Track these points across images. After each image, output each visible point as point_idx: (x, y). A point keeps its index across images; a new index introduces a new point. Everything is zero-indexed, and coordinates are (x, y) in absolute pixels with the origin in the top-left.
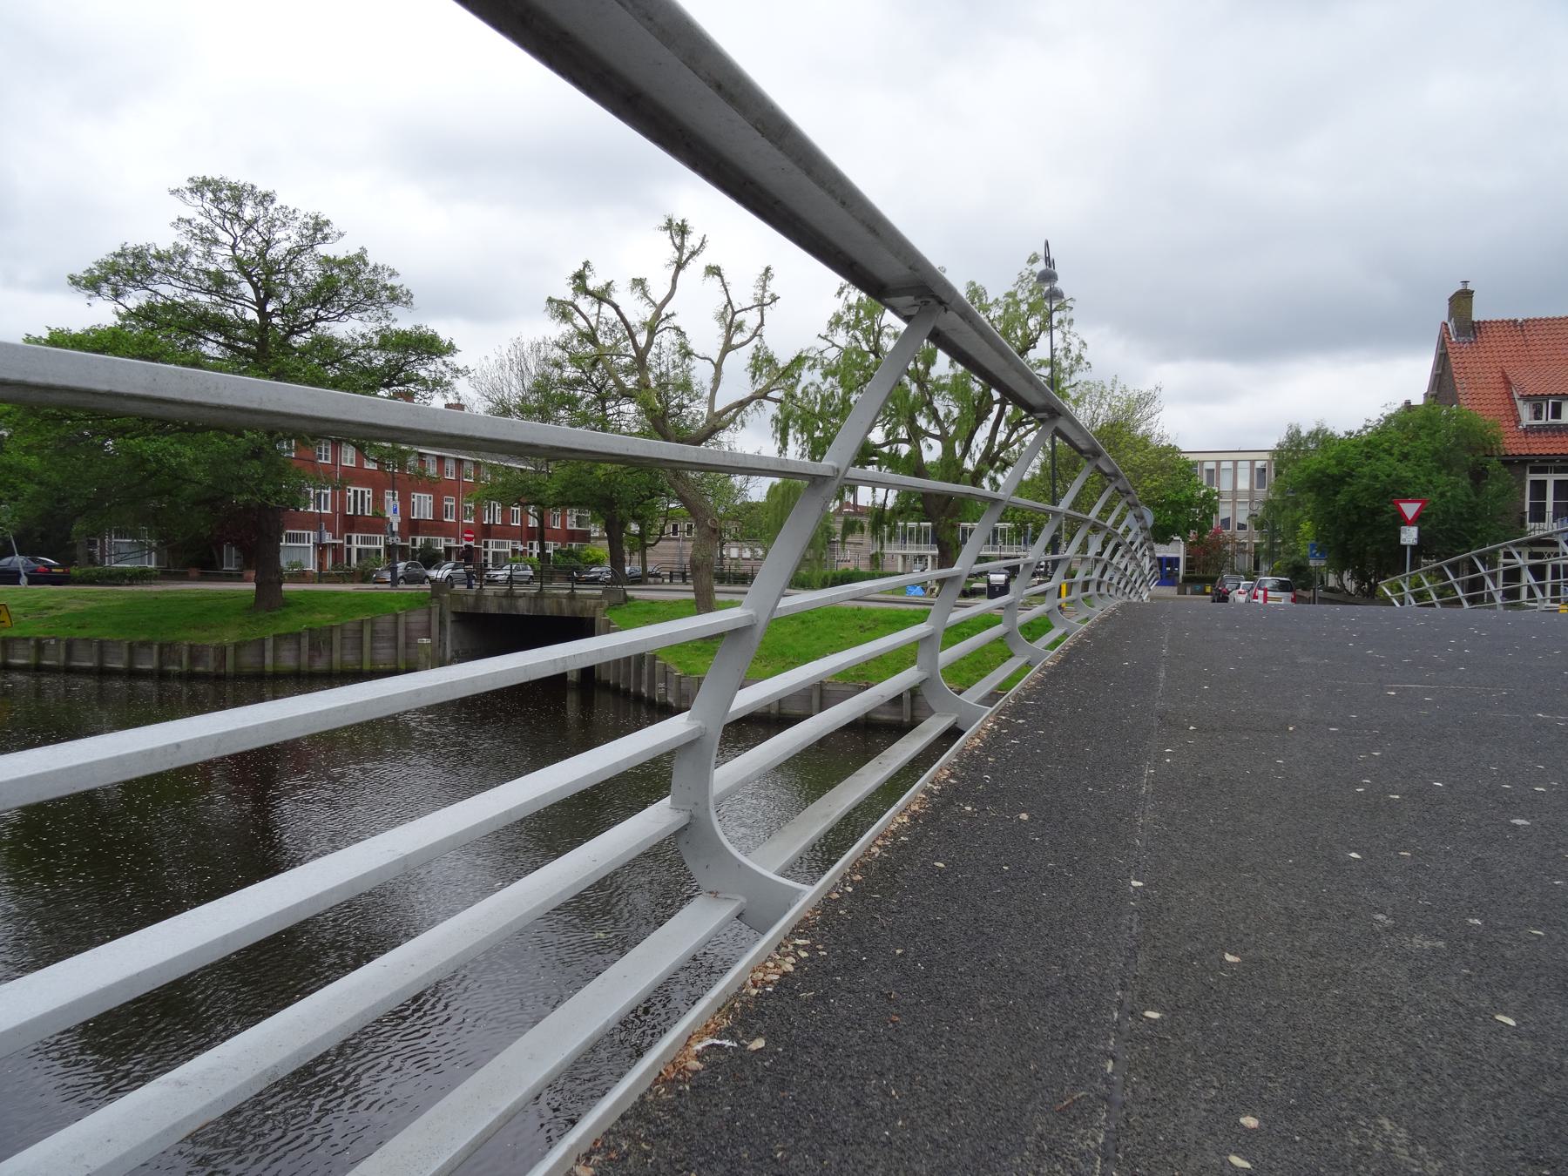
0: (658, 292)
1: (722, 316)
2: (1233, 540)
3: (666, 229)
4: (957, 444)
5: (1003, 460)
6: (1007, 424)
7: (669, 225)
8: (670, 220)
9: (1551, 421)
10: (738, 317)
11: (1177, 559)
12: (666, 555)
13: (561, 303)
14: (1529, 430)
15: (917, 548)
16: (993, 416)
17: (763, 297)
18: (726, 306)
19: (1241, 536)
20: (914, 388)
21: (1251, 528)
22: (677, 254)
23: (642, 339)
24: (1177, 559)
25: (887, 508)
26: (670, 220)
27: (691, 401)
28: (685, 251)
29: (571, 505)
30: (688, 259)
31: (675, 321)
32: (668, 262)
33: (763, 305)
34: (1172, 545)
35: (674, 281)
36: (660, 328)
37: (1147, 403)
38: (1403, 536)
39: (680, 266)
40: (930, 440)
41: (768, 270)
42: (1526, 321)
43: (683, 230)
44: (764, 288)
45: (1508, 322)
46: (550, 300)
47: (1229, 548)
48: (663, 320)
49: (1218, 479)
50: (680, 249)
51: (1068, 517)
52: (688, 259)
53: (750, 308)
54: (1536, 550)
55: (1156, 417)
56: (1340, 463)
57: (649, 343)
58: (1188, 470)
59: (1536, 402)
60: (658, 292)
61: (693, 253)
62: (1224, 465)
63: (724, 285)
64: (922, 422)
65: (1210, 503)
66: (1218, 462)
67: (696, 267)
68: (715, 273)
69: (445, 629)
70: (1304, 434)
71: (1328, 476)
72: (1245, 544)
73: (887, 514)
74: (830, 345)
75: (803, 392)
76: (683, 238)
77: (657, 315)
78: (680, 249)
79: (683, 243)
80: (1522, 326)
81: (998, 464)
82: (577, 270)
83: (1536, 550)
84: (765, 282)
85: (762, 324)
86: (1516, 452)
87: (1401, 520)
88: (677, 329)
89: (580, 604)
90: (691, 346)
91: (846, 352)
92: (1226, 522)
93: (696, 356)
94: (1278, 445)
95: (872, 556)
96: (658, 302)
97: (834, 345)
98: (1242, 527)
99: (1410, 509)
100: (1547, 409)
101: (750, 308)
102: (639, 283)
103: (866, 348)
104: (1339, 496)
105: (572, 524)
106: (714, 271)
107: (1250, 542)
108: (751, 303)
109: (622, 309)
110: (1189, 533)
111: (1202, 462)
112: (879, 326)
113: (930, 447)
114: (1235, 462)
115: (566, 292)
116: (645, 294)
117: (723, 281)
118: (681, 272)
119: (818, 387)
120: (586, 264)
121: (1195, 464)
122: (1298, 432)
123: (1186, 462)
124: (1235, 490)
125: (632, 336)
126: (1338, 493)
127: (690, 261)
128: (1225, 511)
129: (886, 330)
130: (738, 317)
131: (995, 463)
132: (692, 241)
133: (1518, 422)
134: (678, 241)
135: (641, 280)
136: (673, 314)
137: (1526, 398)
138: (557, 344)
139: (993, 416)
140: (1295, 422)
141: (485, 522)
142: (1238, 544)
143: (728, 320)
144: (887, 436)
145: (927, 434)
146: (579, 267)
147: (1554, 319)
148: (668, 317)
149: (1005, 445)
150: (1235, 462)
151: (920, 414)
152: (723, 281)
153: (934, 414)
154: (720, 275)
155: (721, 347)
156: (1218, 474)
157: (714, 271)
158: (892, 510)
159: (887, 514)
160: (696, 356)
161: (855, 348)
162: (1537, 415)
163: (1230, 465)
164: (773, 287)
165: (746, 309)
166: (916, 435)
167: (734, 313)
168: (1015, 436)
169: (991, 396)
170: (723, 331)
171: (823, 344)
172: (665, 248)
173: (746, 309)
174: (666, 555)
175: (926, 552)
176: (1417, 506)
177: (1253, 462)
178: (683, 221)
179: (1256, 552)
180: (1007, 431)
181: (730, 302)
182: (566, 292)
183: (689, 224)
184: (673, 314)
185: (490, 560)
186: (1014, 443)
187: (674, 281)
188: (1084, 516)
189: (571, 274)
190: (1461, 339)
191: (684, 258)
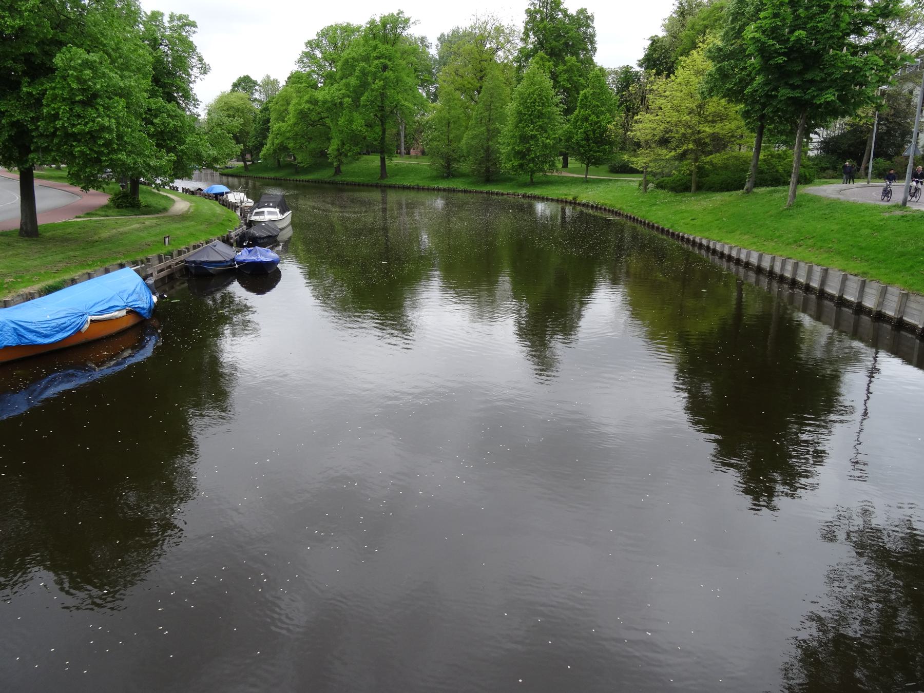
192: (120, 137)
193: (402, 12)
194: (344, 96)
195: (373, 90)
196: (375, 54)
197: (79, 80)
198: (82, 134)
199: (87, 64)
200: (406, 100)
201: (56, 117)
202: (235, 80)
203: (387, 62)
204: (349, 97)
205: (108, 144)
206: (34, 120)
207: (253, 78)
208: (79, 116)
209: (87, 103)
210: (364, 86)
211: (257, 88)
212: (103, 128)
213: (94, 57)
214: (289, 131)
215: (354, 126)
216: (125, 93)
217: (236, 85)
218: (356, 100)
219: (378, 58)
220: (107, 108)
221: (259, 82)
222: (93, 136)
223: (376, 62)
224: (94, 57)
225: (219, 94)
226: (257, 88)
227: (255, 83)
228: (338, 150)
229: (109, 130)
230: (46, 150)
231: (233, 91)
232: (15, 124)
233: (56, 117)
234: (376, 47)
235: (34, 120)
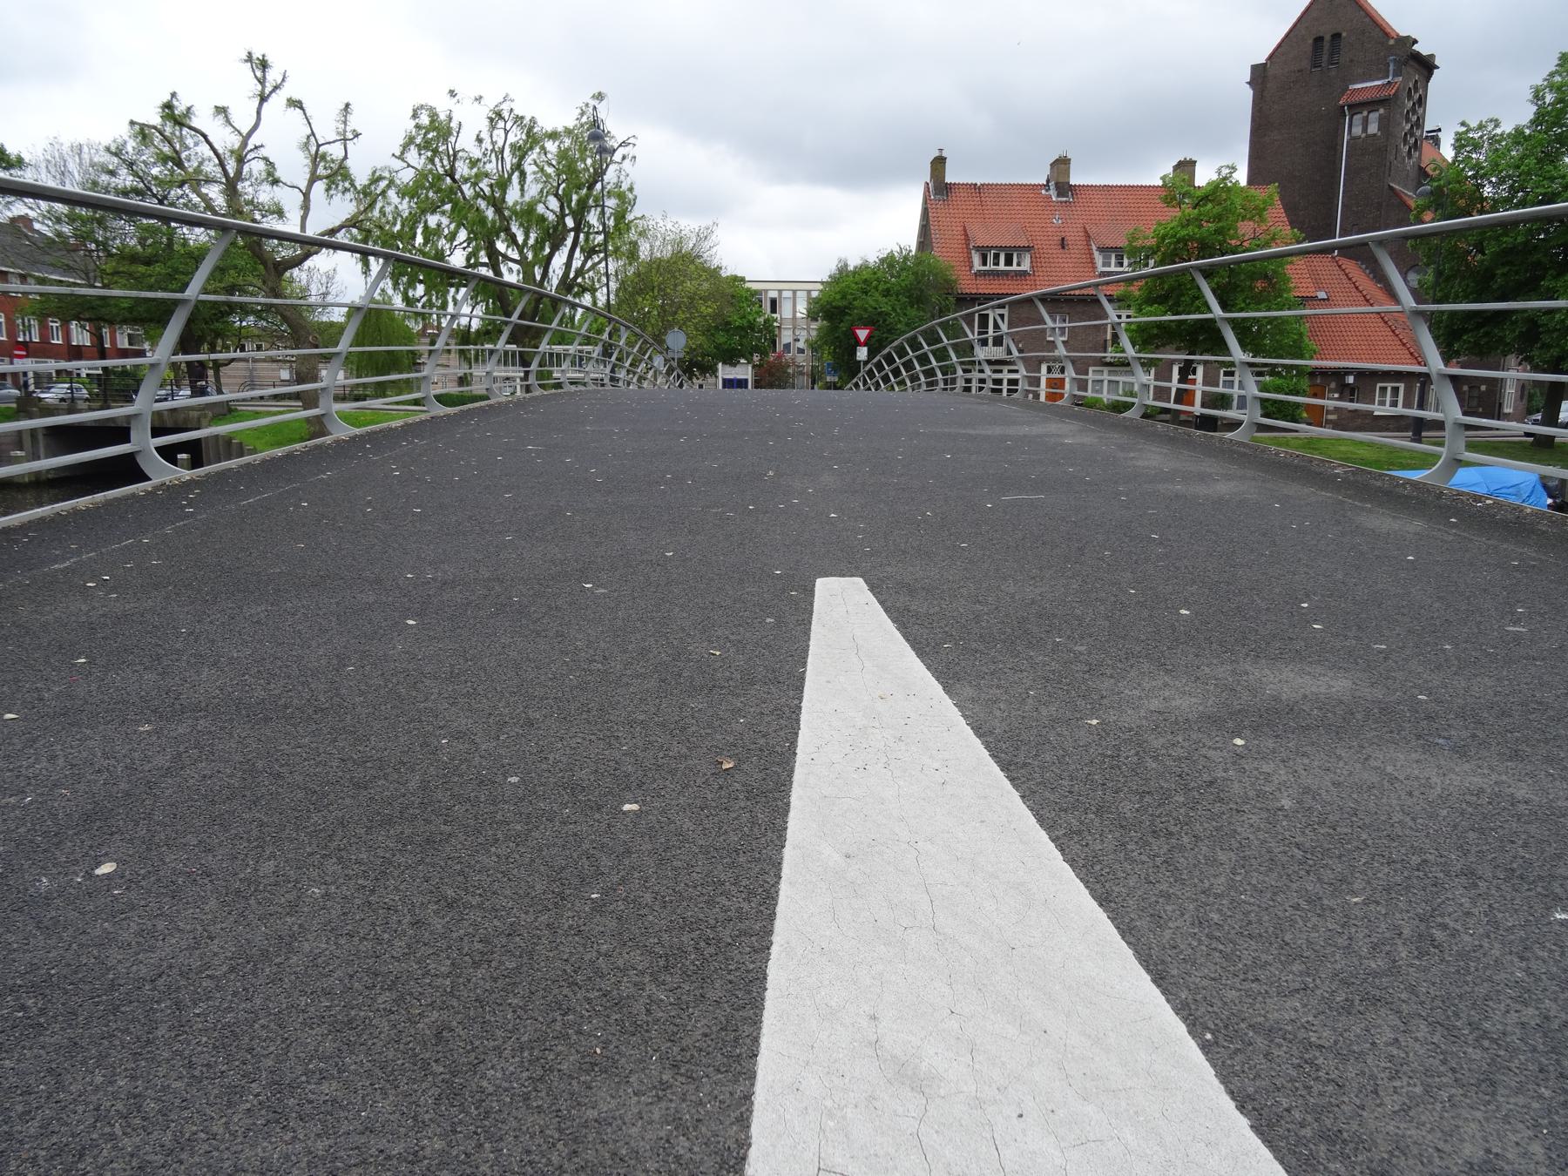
0: (243, 118)
1: (306, 145)
2: (794, 363)
3: (246, 61)
4: (536, 268)
5: (579, 285)
6: (582, 250)
7: (249, 58)
8: (249, 53)
9: (993, 267)
10: (322, 149)
11: (746, 380)
12: (235, 377)
13: (143, 126)
14: (979, 274)
15: (505, 371)
16: (569, 242)
17: (345, 131)
18: (308, 137)
19: (800, 359)
20: (490, 213)
21: (808, 352)
22: (259, 87)
23: (231, 167)
24: (746, 380)
25: (473, 330)
26: (249, 53)
27: (263, 216)
28: (267, 84)
29: (125, 321)
30: (271, 93)
31: (263, 152)
32: (251, 94)
33: (345, 140)
34: (738, 368)
35: (259, 113)
36: (249, 157)
37: (706, 237)
38: (858, 354)
39: (263, 99)
40: (511, 264)
41: (347, 105)
42: (982, 185)
43: (264, 65)
44: (345, 123)
45: (970, 185)
46: (132, 123)
47: (790, 371)
48: (251, 150)
49: (780, 307)
50: (262, 81)
51: (584, 336)
52: (271, 93)
53: (334, 142)
54: (967, 367)
55: (714, 250)
56: (844, 297)
57: (239, 172)
58: (754, 297)
59: (984, 252)
60: (243, 118)
61: (276, 88)
62: (785, 294)
63: (307, 118)
64: (501, 246)
65: (770, 332)
66: (780, 291)
67: (277, 102)
68: (295, 106)
69: (38, 443)
70: (851, 268)
71: (835, 308)
72: (803, 366)
73: (473, 336)
74: (405, 165)
75: (380, 212)
76: (264, 71)
77: (244, 143)
78: (262, 81)
79: (264, 77)
80: (979, 189)
81: (576, 290)
82: (165, 101)
83: (967, 367)
84: (345, 116)
85: (346, 157)
86: (968, 291)
87: (858, 343)
88: (266, 159)
89: (183, 415)
90: (277, 174)
91: (421, 175)
92: (787, 346)
93: (285, 184)
94: (830, 277)
95: (460, 378)
96: (245, 131)
97: (409, 166)
98: (801, 351)
99: (862, 334)
100: (990, 259)
101: (334, 142)
102: (221, 111)
103: (441, 171)
104: (842, 324)
105: (123, 343)
106: (295, 104)
107: (808, 365)
108: (334, 137)
109: (211, 138)
110: (752, 355)
111: (766, 291)
112: (454, 149)
113: (511, 270)
114: (794, 292)
115: (155, 119)
116: (228, 121)
117: (305, 114)
118: (265, 104)
119: (396, 207)
120: (174, 95)
121: (757, 292)
122: (846, 265)
123: (748, 290)
124: (794, 317)
125: (222, 164)
126: (842, 321)
127: (273, 94)
128: (786, 337)
129: (460, 154)
130: (322, 149)
131: (573, 288)
132: (273, 76)
133: (971, 268)
134: (259, 74)
135: (223, 108)
136: (262, 146)
137: (978, 248)
138: (108, 149)
139: (569, 242)
140: (843, 256)
141: (21, 339)
142: (799, 367)
143: (313, 152)
144: (468, 259)
145: (506, 258)
146: (167, 98)
147: (997, 185)
148: (256, 148)
149: (580, 272)
150: (794, 292)
151: (498, 239)
152: (305, 114)
153: (512, 240)
154: (301, 108)
155: (308, 176)
156: (780, 302)
157: (295, 104)
158: (478, 331)
159: (473, 336)
160: (285, 184)
161: (430, 171)
162: (984, 263)
163: (789, 294)
164: (354, 122)
165: (329, 143)
166: (495, 259)
167: (319, 146)
168: (589, 264)
169: (565, 224)
170: (308, 161)
171: (398, 164)
172: (248, 82)
173: (329, 143)
174: (235, 377)
175: (513, 374)
176: (858, 332)
177: (809, 292)
178: (264, 56)
179: (812, 373)
180: (582, 258)
181: (313, 134)
182: (155, 119)
183: (269, 59)
184: (262, 146)
185: (31, 381)
186: (589, 270)
187: (259, 113)
188: (178, 296)
189: (160, 103)
190: (937, 197)
191: (267, 91)
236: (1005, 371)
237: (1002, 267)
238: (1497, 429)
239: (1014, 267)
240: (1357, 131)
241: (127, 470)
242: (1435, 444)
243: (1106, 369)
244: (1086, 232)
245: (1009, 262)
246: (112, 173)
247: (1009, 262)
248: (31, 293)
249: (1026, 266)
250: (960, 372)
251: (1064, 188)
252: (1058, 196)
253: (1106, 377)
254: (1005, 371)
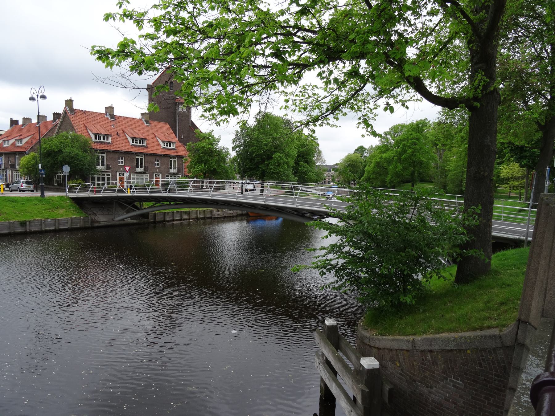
162: (96, 139)
192: (284, 173)
193: (427, 119)
194: (394, 156)
195: (408, 153)
196: (410, 138)
197: (277, 161)
198: (276, 172)
199: (280, 157)
200: (424, 158)
201: (271, 169)
202: (356, 148)
203: (416, 141)
204: (397, 156)
205: (281, 175)
206: (267, 169)
207: (365, 147)
208: (276, 169)
209: (278, 166)
210: (404, 151)
211: (366, 151)
212: (280, 171)
213: (281, 155)
214: (371, 171)
215: (397, 169)
216: (287, 163)
217: (356, 150)
218: (400, 159)
219: (411, 139)
220: (282, 167)
221: (367, 148)
222: (278, 173)
223: (410, 141)
224: (281, 155)
225: (347, 154)
226: (366, 151)
227: (365, 149)
228: (390, 180)
229: (281, 171)
230: (268, 176)
231: (355, 153)
232: (263, 170)
233: (271, 169)
234: (411, 134)
235: (267, 169)
236: (106, 175)
237: (102, 140)
238: (182, 183)
239: (106, 141)
240: (181, 110)
241: (293, 195)
242: (156, 378)
243: (136, 174)
244: (123, 131)
245: (104, 139)
246: (507, 281)
247: (104, 139)
248: (328, 215)
249: (109, 141)
250: (160, 185)
251: (112, 116)
252: (111, 118)
253: (136, 177)
254: (106, 175)
